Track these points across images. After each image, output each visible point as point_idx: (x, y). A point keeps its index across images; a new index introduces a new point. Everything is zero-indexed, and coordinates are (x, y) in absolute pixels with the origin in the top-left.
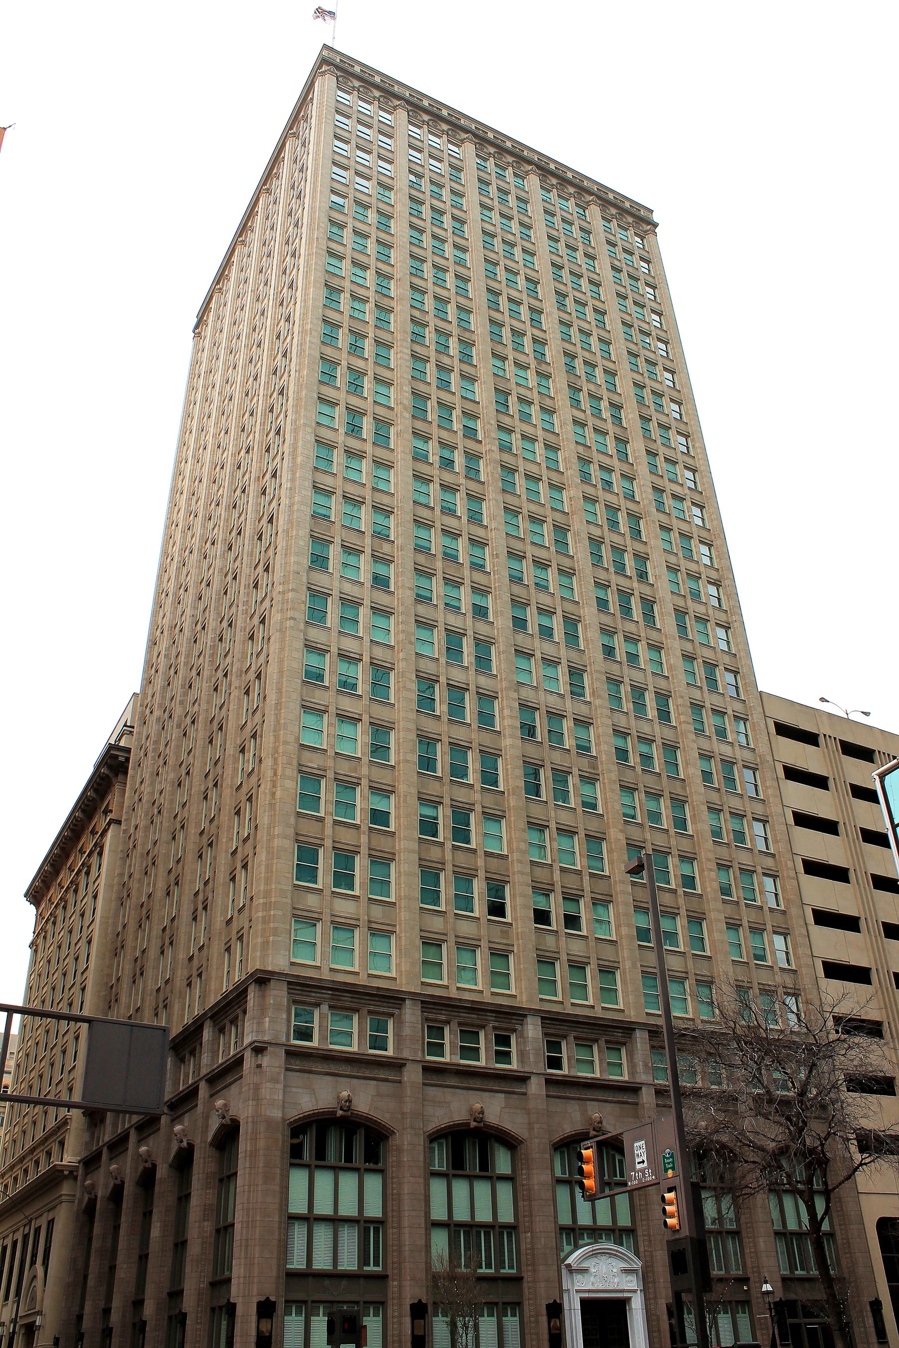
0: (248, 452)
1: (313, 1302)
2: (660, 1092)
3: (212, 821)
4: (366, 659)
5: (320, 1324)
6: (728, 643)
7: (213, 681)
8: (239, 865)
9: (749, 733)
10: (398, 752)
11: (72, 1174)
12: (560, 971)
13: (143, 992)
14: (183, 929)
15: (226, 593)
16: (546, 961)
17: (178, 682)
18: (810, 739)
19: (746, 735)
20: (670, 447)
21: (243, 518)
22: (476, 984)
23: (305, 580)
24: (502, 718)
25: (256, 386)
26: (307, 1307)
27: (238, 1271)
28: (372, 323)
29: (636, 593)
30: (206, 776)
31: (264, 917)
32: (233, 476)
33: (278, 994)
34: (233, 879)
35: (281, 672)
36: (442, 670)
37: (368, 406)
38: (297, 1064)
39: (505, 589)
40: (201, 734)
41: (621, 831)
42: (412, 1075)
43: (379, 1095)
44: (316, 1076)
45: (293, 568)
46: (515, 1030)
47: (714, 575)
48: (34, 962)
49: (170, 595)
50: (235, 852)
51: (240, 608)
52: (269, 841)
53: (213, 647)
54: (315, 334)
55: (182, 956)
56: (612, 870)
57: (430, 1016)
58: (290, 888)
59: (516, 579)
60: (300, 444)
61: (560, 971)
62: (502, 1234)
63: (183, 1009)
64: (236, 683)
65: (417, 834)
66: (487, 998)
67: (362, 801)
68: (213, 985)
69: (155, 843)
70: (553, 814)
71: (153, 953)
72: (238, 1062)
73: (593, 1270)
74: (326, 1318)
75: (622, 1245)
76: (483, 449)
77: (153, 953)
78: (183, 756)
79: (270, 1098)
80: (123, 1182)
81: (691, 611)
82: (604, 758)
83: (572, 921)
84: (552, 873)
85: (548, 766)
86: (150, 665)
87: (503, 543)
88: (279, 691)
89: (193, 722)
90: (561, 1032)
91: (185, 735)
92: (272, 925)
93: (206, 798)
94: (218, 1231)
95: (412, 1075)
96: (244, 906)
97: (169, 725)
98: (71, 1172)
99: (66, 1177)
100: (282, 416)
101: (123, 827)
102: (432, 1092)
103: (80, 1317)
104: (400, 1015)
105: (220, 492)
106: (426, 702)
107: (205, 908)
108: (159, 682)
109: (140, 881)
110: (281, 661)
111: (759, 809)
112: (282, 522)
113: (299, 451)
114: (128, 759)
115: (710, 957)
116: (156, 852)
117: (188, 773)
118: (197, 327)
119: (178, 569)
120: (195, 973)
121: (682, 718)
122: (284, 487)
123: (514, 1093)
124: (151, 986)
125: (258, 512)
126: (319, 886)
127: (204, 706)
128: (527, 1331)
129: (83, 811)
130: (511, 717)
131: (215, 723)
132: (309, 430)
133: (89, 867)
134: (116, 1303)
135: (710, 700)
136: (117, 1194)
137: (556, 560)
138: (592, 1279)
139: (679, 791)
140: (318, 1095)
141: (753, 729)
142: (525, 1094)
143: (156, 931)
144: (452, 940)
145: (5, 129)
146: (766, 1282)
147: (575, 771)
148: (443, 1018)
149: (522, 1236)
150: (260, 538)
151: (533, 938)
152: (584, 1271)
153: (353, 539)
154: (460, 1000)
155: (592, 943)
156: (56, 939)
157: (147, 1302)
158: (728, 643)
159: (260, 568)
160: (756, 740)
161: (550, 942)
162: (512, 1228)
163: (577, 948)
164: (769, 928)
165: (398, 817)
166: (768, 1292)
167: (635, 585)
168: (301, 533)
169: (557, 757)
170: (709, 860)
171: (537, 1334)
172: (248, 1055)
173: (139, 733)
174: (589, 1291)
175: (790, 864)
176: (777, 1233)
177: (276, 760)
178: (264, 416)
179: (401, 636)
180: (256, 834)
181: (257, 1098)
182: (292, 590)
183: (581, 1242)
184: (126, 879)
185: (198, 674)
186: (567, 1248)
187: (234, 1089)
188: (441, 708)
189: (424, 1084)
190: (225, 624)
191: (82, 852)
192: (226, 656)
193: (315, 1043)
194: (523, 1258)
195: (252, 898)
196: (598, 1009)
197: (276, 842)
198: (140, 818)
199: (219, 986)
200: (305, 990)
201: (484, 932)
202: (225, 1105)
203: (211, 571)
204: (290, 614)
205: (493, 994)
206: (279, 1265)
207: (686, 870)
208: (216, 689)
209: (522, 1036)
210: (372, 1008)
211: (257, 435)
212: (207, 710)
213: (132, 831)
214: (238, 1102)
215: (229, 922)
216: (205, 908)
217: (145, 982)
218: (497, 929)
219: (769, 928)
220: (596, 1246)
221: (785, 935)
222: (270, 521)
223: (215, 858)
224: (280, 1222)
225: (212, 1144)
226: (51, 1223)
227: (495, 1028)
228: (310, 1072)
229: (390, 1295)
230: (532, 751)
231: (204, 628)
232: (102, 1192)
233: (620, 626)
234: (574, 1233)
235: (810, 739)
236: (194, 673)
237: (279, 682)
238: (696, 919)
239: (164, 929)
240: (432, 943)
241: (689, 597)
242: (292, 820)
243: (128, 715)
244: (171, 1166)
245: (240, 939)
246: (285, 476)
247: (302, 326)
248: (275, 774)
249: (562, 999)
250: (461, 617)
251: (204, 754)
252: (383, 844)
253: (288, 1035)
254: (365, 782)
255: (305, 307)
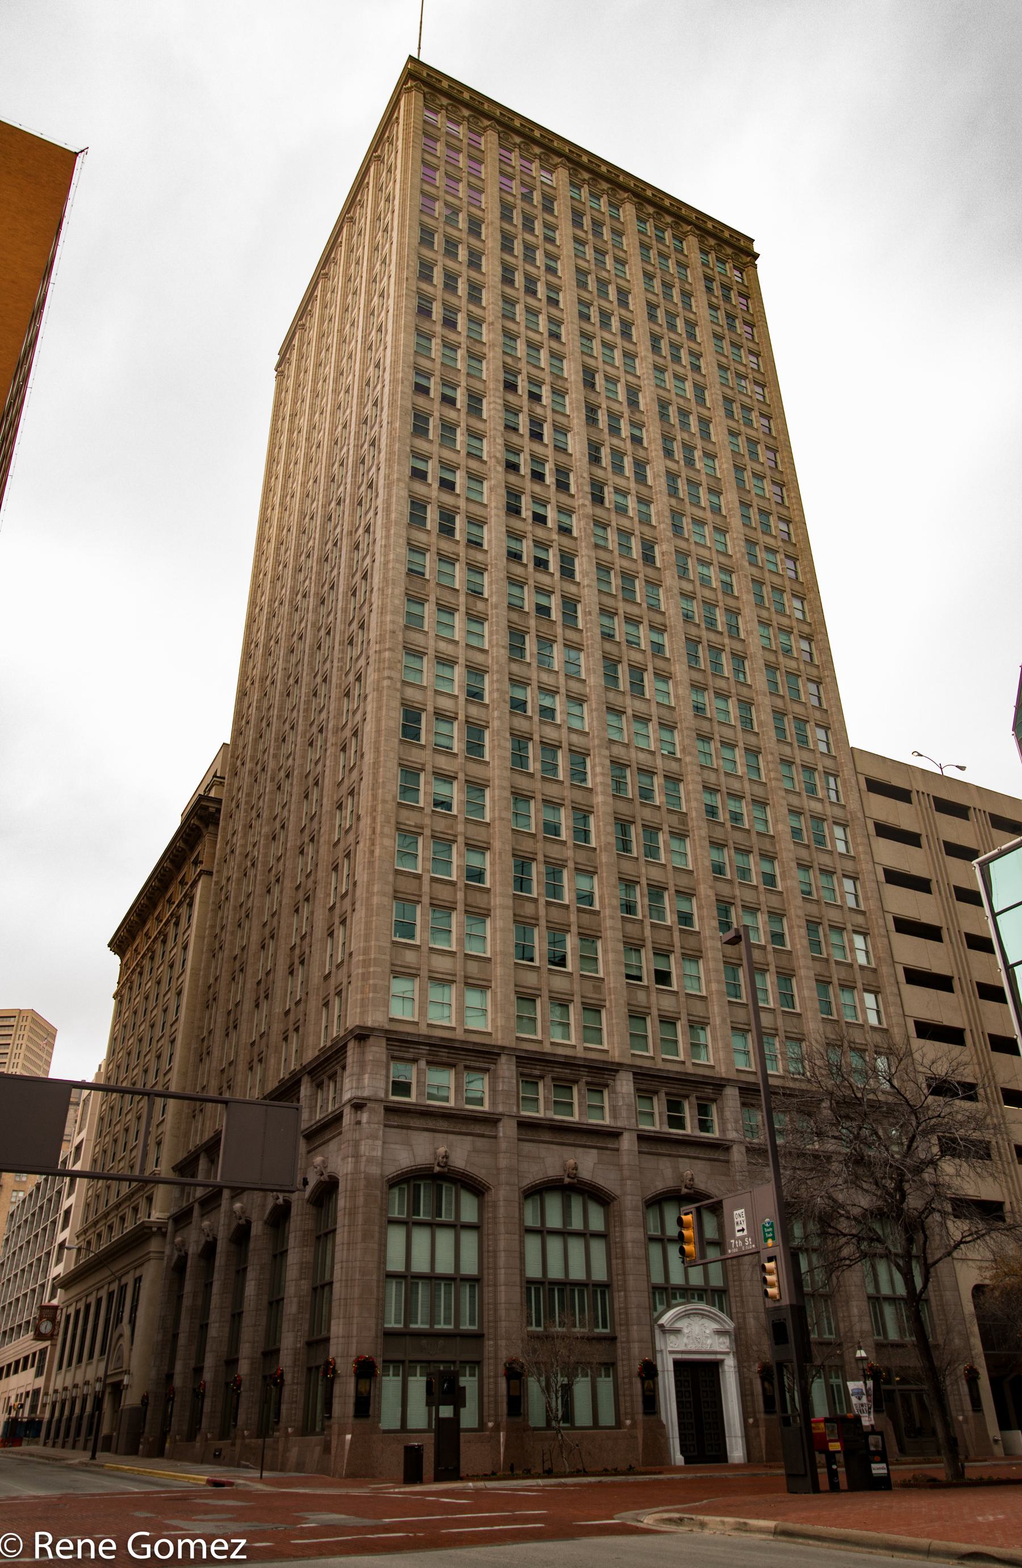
0: (339, 504)
1: (411, 1362)
2: (751, 1150)
3: (308, 876)
4: (461, 717)
5: (418, 1385)
6: (819, 698)
7: (308, 736)
8: (337, 921)
9: (840, 789)
10: (493, 810)
11: (161, 1231)
12: (652, 1027)
13: (237, 1045)
14: (279, 984)
15: (319, 648)
16: (637, 1015)
17: (271, 735)
18: (903, 795)
19: (837, 792)
20: (741, 363)
21: (335, 572)
22: (567, 1038)
23: (400, 638)
24: (594, 775)
25: (346, 434)
26: (404, 1367)
27: (337, 1328)
28: (464, 371)
29: (727, 649)
30: (302, 830)
31: (363, 974)
32: (323, 528)
33: (376, 1050)
34: (331, 934)
35: (378, 732)
36: (536, 727)
37: (461, 459)
38: (395, 1120)
39: (597, 646)
40: (295, 790)
41: (711, 887)
42: (507, 1130)
43: (475, 1150)
44: (416, 1133)
45: (389, 627)
46: (607, 1086)
47: (806, 629)
48: (118, 1013)
49: (261, 646)
50: (332, 908)
51: (335, 664)
52: (367, 899)
53: (308, 702)
54: (406, 383)
55: (278, 1010)
56: (701, 925)
57: (526, 1071)
58: (389, 945)
59: (608, 636)
60: (394, 499)
61: (652, 1027)
62: (595, 1292)
63: (279, 1063)
64: (331, 739)
65: (511, 891)
66: (580, 1053)
67: (457, 857)
68: (311, 1040)
69: (249, 896)
70: (643, 870)
71: (247, 1006)
72: (338, 1118)
73: (686, 1331)
74: (425, 1379)
75: (714, 1305)
76: (576, 503)
77: (247, 1006)
78: (278, 810)
79: (365, 1154)
80: (215, 1239)
81: (782, 667)
82: (694, 814)
83: (663, 977)
84: (643, 929)
85: (639, 822)
86: (239, 715)
87: (596, 599)
88: (377, 750)
89: (287, 776)
90: (651, 1088)
91: (279, 788)
92: (371, 982)
93: (302, 852)
94: (315, 1289)
95: (507, 1130)
96: (342, 962)
97: (262, 778)
98: (159, 1228)
99: (154, 1233)
100: (374, 469)
101: (214, 878)
102: (527, 1147)
103: (170, 1377)
104: (495, 1070)
105: (311, 543)
106: (519, 759)
107: (302, 962)
108: (251, 733)
109: (233, 933)
110: (378, 720)
111: (849, 866)
112: (376, 580)
113: (394, 507)
114: (219, 811)
115: (800, 1015)
116: (250, 904)
117: (283, 827)
118: (279, 365)
119: (268, 620)
120: (291, 1028)
121: (772, 775)
122: (378, 543)
123: (606, 1149)
124: (245, 1039)
125: (351, 567)
126: (417, 942)
127: (298, 762)
128: (621, 1392)
129: (172, 861)
130: (603, 774)
131: (311, 779)
132: (402, 485)
133: (178, 918)
134: (209, 1361)
135: (800, 756)
136: (209, 1251)
137: (647, 616)
138: (685, 1340)
139: (769, 847)
140: (418, 1149)
141: (844, 786)
142: (617, 1150)
143: (250, 985)
144: (545, 994)
145: (77, 154)
146: (860, 1348)
147: (666, 828)
148: (537, 1072)
149: (616, 1294)
150: (354, 594)
151: (625, 993)
152: (678, 1331)
153: (448, 598)
154: (555, 1055)
155: (683, 999)
156: (143, 990)
157: (205, 1370)
158: (819, 698)
159: (355, 626)
160: (846, 796)
161: (641, 996)
162: (605, 1287)
163: (667, 1004)
164: (859, 985)
165: (493, 874)
166: (862, 1359)
167: (727, 641)
168: (397, 591)
169: (647, 813)
170: (798, 917)
171: (631, 1396)
172: (347, 1110)
173: (230, 784)
174: (682, 1352)
175: (881, 922)
176: (869, 1298)
177: (374, 819)
178: (356, 468)
179: (496, 695)
180: (354, 891)
181: (357, 1156)
182: (390, 649)
183: (674, 1302)
184: (218, 930)
185: (292, 728)
186: (660, 1308)
187: (333, 1145)
188: (534, 766)
189: (519, 1140)
190: (319, 679)
191: (170, 902)
192: (320, 712)
193: (413, 1099)
194: (617, 1318)
195: (351, 954)
196: (688, 1064)
197: (375, 900)
198: (233, 869)
199: (317, 1039)
200: (402, 1044)
201: (576, 987)
202: (324, 1162)
203: (303, 625)
204: (386, 673)
205: (586, 1049)
206: (377, 1325)
207: (766, 867)
208: (311, 744)
209: (614, 1092)
210: (468, 1063)
211: (348, 487)
212: (302, 766)
213: (224, 882)
214: (337, 1159)
215: (327, 978)
216: (302, 962)
217: (239, 1037)
218: (589, 984)
219: (859, 985)
220: (689, 1307)
221: (876, 993)
222: (365, 577)
223: (312, 913)
224: (378, 1281)
225: (309, 1201)
226: (138, 1280)
227: (587, 1083)
228: (409, 1128)
229: (486, 1354)
230: (623, 808)
231: (297, 682)
232: (193, 1249)
233: (711, 683)
234: (666, 1293)
235: (903, 795)
236: (287, 726)
237: (377, 742)
238: (786, 976)
239: (259, 983)
240: (526, 998)
241: (780, 652)
242: (391, 878)
243: (218, 766)
244: (266, 1223)
245: (339, 994)
246: (379, 533)
247: (393, 373)
248: (374, 833)
249: (651, 1054)
250: (553, 675)
251: (299, 810)
252: (480, 900)
253: (387, 1091)
254: (460, 839)
255: (395, 353)
